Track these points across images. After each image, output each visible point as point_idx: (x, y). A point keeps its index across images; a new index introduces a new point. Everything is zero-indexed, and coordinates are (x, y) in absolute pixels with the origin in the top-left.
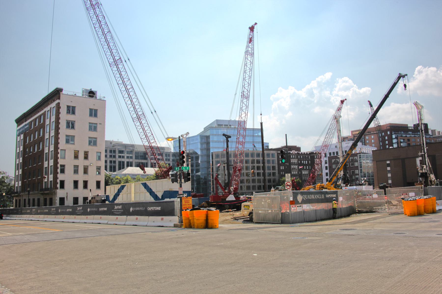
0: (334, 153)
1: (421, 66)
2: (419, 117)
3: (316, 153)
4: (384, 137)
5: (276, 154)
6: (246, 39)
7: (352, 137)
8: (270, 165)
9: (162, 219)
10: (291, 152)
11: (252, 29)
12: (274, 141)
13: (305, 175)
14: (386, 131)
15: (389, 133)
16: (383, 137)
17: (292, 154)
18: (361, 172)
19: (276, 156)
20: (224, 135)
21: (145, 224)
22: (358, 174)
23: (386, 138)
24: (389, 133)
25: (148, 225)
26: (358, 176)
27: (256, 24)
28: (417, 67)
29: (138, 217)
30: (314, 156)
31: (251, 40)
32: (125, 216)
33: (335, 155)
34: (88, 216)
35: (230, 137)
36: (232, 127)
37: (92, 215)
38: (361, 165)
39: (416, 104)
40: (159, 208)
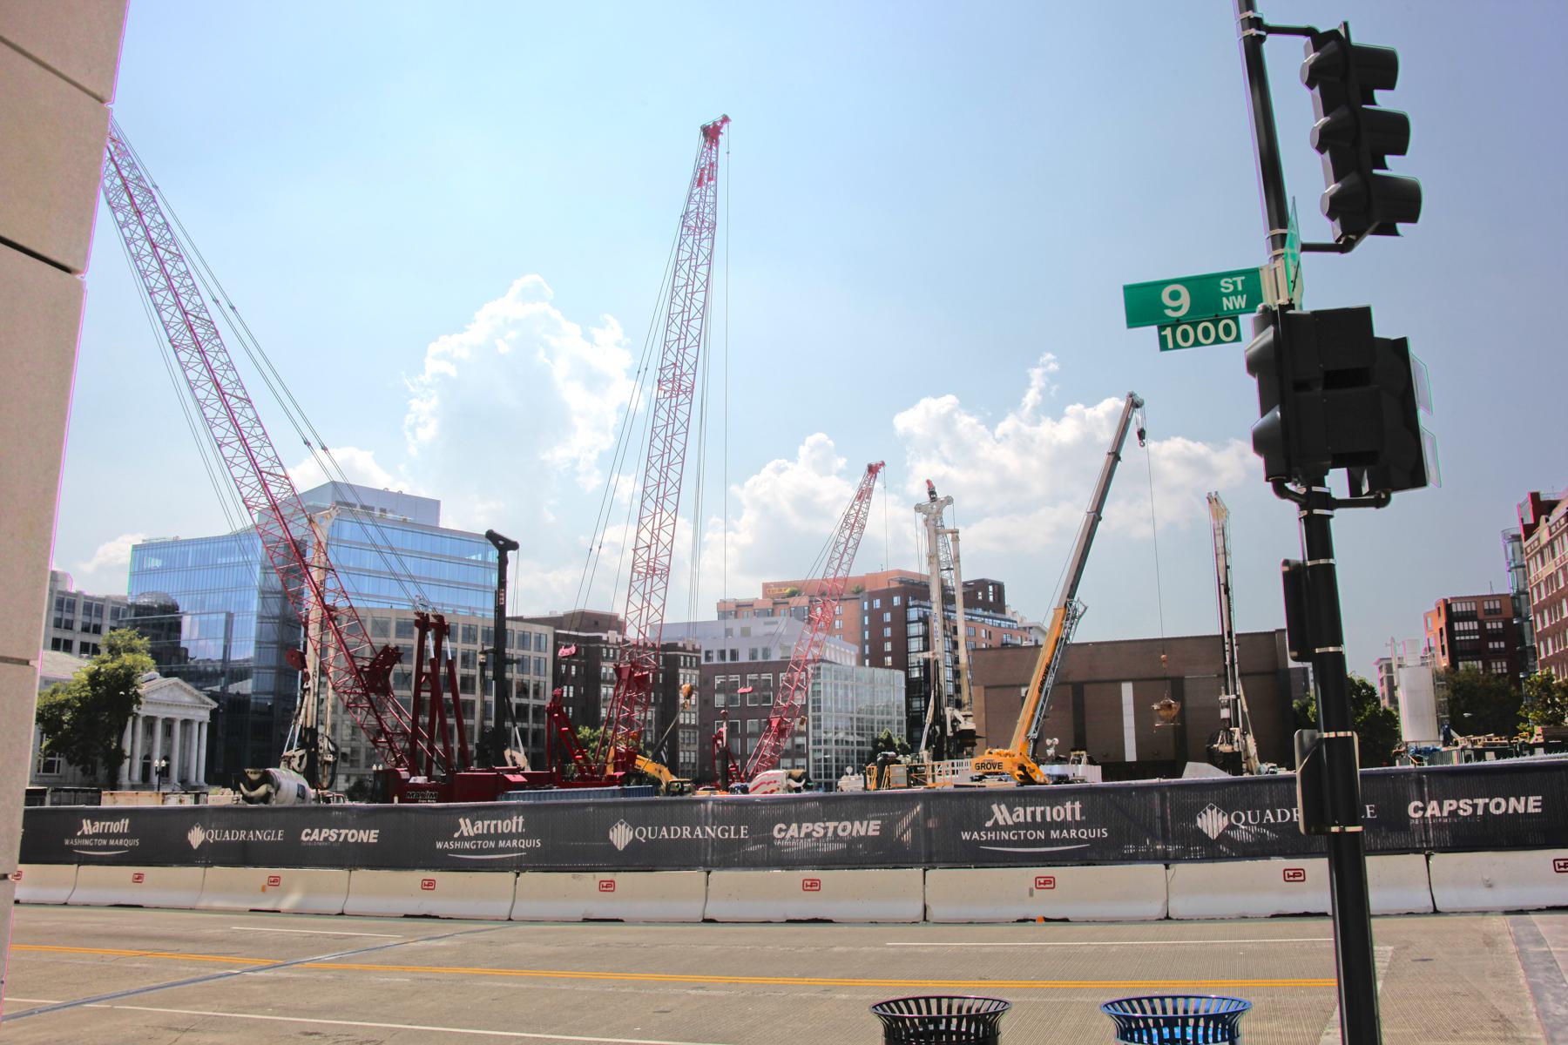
0: (722, 654)
1: (949, 400)
2: (1220, 544)
3: (684, 649)
4: (880, 613)
5: (551, 638)
6: (688, 174)
7: (769, 605)
8: (526, 677)
9: (139, 878)
10: (605, 637)
11: (711, 134)
12: (538, 591)
13: (689, 726)
14: (886, 596)
15: (897, 601)
16: (876, 616)
17: (607, 642)
18: (817, 727)
19: (550, 646)
20: (492, 536)
21: (62, 895)
22: (806, 734)
23: (888, 617)
24: (897, 601)
25: (74, 899)
26: (800, 740)
27: (725, 119)
28: (1024, 395)
29: (430, 875)
30: (677, 658)
31: (705, 176)
32: (343, 873)
33: (728, 660)
34: (621, 878)
35: (515, 546)
36: (390, 516)
37: (341, 866)
38: (817, 701)
39: (1213, 500)
40: (370, 836)
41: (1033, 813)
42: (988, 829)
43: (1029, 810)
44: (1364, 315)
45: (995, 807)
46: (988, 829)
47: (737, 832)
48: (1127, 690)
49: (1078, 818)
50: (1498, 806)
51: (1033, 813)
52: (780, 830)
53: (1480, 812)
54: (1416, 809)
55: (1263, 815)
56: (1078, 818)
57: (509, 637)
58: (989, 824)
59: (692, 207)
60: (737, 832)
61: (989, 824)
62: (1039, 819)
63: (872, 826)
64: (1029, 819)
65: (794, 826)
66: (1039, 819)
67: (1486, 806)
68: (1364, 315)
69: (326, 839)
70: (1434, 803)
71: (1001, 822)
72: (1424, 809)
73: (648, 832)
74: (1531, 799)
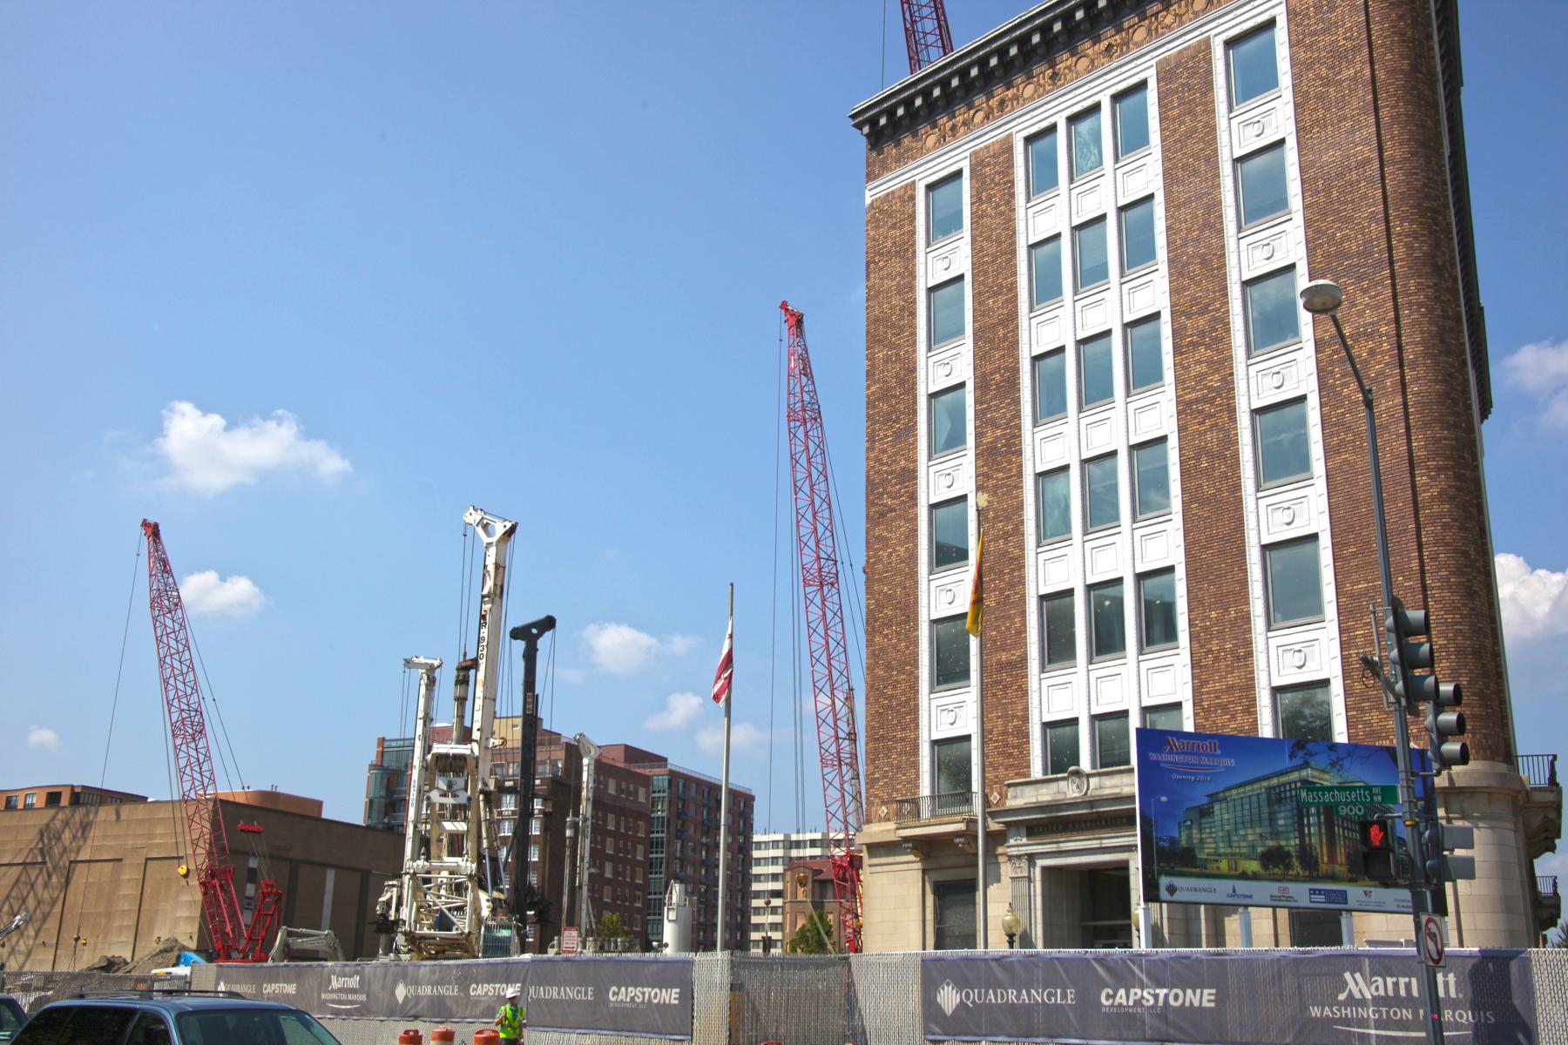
41: (1396, 985)
42: (1340, 1004)
43: (1390, 981)
44: (319, 804)
45: (1347, 975)
46: (1340, 1004)
47: (1064, 996)
48: (331, 875)
49: (1453, 994)
50: (1176, 997)
51: (1396, 985)
52: (1108, 997)
53: (1161, 1003)
54: (1108, 997)
55: (987, 993)
56: (1453, 994)
57: (1066, 664)
58: (1342, 997)
59: (171, 694)
60: (1064, 996)
61: (1342, 997)
62: (1403, 993)
63: (1206, 997)
64: (1391, 993)
65: (1122, 992)
66: (1403, 993)
67: (1166, 996)
68: (319, 804)
69: (1138, 1003)
70: (1122, 992)
71: (1357, 996)
72: (1114, 997)
73: (974, 994)
74: (1206, 992)
